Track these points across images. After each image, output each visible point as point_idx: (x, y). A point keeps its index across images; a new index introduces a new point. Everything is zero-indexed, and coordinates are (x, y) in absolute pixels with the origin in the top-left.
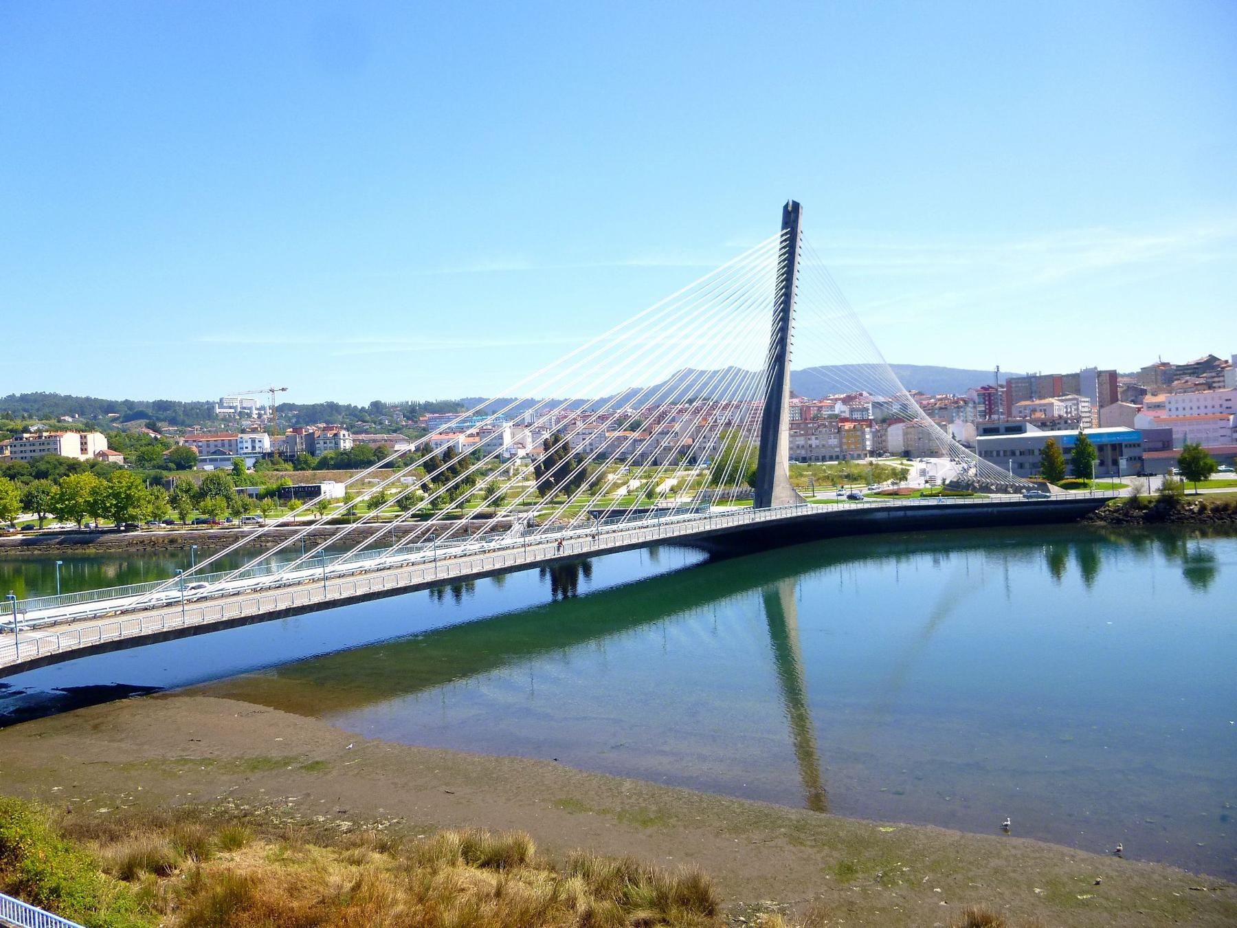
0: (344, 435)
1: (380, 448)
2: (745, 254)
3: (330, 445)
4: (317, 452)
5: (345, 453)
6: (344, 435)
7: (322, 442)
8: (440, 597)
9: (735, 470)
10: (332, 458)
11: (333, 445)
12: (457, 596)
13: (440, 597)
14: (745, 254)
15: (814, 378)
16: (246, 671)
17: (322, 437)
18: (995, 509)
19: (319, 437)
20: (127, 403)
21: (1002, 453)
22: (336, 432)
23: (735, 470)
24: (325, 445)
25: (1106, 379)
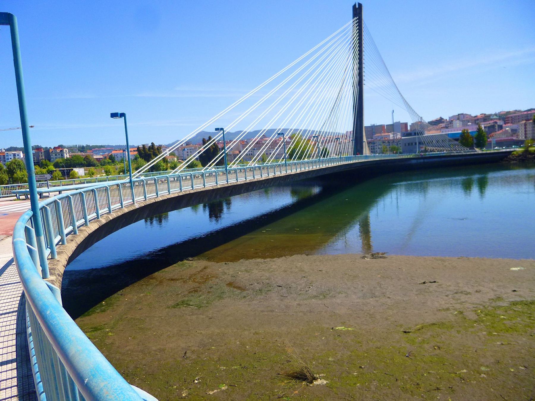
0: (66, 151)
1: (87, 156)
2: (295, 95)
3: (59, 156)
4: (52, 160)
5: (67, 159)
6: (66, 151)
7: (54, 155)
8: (151, 223)
9: (303, 152)
10: (61, 163)
11: (60, 156)
12: (481, 196)
13: (151, 223)
14: (295, 95)
15: (374, 129)
16: (36, 306)
17: (54, 152)
18: (463, 158)
19: (52, 152)
20: (108, 146)
21: (407, 145)
22: (62, 149)
23: (303, 152)
24: (56, 156)
25: (404, 126)
